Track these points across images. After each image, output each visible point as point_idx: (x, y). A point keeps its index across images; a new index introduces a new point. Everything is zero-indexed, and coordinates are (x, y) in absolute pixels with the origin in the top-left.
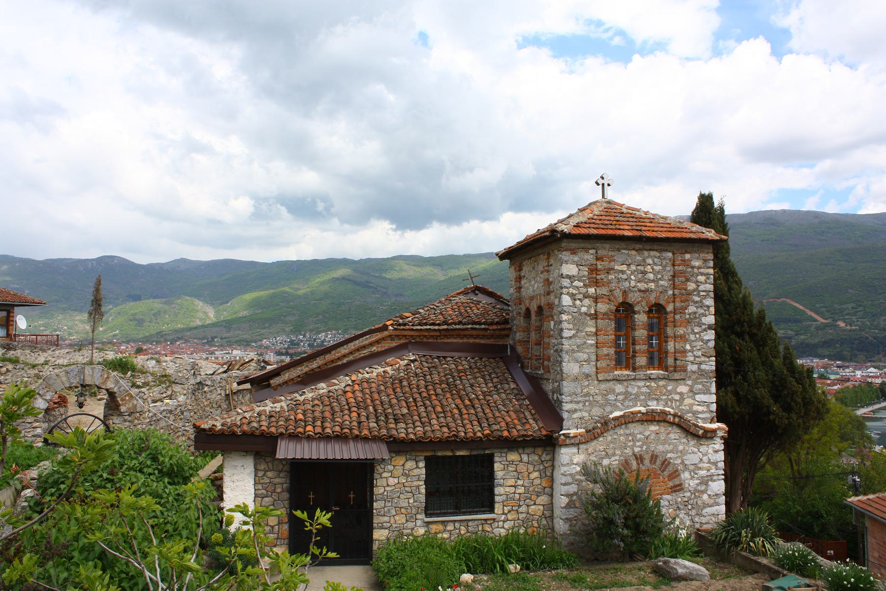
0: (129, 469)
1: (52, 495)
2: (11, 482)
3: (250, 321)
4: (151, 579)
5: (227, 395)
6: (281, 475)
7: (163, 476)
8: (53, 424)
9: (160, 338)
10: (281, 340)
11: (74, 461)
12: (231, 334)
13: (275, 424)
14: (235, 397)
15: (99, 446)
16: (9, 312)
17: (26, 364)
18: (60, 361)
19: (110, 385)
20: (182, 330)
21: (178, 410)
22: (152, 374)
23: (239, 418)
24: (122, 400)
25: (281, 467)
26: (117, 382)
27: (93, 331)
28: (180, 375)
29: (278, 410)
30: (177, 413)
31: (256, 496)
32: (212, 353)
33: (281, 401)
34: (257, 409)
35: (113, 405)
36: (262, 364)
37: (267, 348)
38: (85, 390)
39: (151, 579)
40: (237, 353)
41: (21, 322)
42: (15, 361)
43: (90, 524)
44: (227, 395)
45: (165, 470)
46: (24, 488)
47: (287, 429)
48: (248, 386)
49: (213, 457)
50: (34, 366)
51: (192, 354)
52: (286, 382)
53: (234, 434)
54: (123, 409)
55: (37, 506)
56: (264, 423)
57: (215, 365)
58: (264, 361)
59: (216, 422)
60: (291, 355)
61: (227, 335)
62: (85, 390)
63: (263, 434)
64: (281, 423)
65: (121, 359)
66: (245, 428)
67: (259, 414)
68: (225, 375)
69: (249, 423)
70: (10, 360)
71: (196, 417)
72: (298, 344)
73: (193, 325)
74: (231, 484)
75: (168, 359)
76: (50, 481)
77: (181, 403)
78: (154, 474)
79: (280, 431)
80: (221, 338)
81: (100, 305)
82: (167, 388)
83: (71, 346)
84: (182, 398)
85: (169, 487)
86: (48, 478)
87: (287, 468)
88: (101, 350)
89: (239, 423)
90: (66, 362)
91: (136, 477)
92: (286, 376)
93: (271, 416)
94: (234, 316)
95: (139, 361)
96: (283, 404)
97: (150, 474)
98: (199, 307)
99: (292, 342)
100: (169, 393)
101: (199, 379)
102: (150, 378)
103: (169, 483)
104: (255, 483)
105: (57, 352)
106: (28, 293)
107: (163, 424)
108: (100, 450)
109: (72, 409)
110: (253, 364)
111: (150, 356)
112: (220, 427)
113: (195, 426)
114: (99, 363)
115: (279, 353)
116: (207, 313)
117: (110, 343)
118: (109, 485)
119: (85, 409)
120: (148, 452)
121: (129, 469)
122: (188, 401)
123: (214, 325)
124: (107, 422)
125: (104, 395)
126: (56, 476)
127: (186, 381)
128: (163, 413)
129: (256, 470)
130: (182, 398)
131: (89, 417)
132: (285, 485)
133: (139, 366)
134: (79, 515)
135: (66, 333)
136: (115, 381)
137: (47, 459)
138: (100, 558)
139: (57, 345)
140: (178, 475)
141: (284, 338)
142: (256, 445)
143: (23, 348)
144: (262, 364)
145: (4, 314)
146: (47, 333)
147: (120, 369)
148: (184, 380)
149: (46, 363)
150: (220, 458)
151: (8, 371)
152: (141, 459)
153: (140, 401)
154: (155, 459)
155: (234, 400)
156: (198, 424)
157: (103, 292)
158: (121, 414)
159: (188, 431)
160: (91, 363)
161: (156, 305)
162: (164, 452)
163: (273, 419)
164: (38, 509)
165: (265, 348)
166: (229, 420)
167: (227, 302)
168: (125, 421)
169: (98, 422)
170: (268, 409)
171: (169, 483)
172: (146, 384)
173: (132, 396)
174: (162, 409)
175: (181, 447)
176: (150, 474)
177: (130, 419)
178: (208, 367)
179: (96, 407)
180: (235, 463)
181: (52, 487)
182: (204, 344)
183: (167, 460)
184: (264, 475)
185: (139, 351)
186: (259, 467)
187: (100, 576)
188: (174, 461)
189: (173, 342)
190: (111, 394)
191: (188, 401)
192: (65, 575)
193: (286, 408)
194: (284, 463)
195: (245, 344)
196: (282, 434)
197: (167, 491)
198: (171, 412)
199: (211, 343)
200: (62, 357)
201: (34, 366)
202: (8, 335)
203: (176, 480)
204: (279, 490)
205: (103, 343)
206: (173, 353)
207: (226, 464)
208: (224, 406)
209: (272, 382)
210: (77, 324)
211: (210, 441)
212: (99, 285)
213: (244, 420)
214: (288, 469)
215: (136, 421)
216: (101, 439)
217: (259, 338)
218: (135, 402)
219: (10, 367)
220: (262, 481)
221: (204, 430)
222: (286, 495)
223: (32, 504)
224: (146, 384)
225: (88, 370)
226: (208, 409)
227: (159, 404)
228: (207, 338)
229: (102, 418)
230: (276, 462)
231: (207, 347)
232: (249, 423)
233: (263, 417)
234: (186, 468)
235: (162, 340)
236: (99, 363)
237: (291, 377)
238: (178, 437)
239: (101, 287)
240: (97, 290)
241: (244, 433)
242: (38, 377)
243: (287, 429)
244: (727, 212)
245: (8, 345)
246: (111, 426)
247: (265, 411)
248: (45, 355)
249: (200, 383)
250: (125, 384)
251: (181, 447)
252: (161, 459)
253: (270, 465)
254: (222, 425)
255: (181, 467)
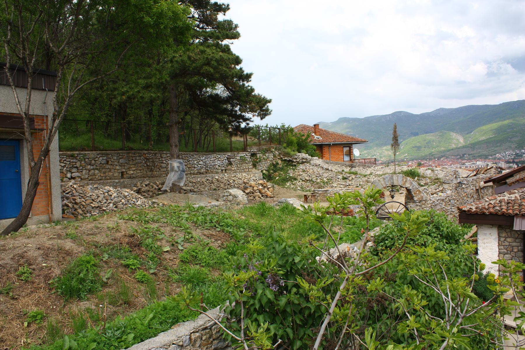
0: (423, 233)
1: (382, 246)
2: (362, 238)
3: (487, 143)
4: (446, 299)
5: (477, 190)
6: (517, 241)
7: (443, 238)
8: (378, 207)
9: (431, 157)
10: (509, 154)
11: (405, 230)
12: (475, 151)
13: (511, 208)
14: (482, 191)
15: (419, 222)
16: (350, 148)
17: (361, 175)
18: (378, 173)
19: (408, 185)
20: (444, 151)
21: (447, 199)
22: (429, 178)
23: (487, 204)
24: (415, 194)
25: (517, 235)
26: (411, 183)
27: (395, 155)
28: (448, 178)
29: (513, 199)
30: (447, 201)
31: (500, 253)
32: (464, 164)
33: (515, 193)
34: (499, 199)
35: (410, 196)
36: (499, 170)
37: (499, 159)
38: (394, 188)
39: (446, 299)
40: (480, 163)
41: (356, 152)
42: (356, 174)
43: (409, 265)
44: (477, 190)
45: (444, 235)
46: (368, 241)
47: (520, 211)
48: (491, 184)
49: (470, 227)
50: (365, 176)
51: (451, 165)
52: (517, 181)
53: (484, 214)
54: (415, 199)
55: (375, 252)
56: (504, 207)
57: (467, 171)
58: (500, 168)
59: (472, 206)
60: (517, 164)
61: (472, 152)
62: (394, 188)
63: (503, 214)
64: (515, 207)
65: (411, 170)
66: (491, 210)
67: (500, 202)
68: (475, 177)
69: (494, 207)
70: (353, 173)
71: (458, 203)
72: (521, 156)
73: (450, 147)
74: (483, 245)
75: (438, 169)
76: (380, 238)
77: (449, 195)
78: (437, 237)
79: (515, 212)
80: (469, 155)
81: (397, 140)
82: (439, 186)
83: (382, 164)
84: (449, 192)
85: (447, 245)
86: (379, 237)
87: (521, 236)
88: (399, 165)
89: (487, 207)
90: (381, 173)
91: (427, 238)
92: (517, 177)
93: (508, 203)
94: (476, 141)
95: (421, 171)
96: (517, 195)
97: (435, 237)
98: (454, 137)
99: (517, 154)
100: (441, 188)
101: (459, 181)
102: (428, 181)
103: (446, 243)
104: (499, 245)
105: (376, 168)
106: (358, 137)
107: (438, 207)
108: (419, 224)
109: (387, 199)
110: (493, 170)
111: (427, 168)
112: (474, 210)
113: (458, 208)
114: (399, 173)
115: (508, 162)
116: (458, 140)
117: (403, 161)
118: (412, 242)
119: (394, 199)
120: (433, 224)
121: (423, 233)
122: (453, 194)
123: (464, 147)
124: (407, 206)
125: (405, 192)
126: (383, 236)
127: (450, 183)
128: (440, 201)
129: (499, 237)
130: (449, 192)
131: (396, 205)
132: (519, 248)
133: (421, 174)
134: (403, 259)
135: (379, 157)
136: (410, 183)
137: (378, 226)
138: (410, 283)
139: (376, 164)
140: (451, 238)
141: (511, 152)
142: (501, 221)
143: (359, 166)
144: (499, 170)
145: (348, 149)
146: (369, 157)
147: (411, 176)
148: (450, 181)
149: (371, 174)
150: (474, 228)
151: (352, 179)
152: (430, 228)
153: (425, 194)
154: (437, 228)
155: (481, 193)
156: (460, 207)
157: (398, 133)
158: (414, 202)
159: (453, 212)
160: (395, 173)
161: (427, 137)
162: (443, 224)
163: (510, 205)
164: (375, 253)
165: (498, 159)
166: (480, 205)
167: (471, 132)
168: (417, 205)
169: (402, 206)
170: (506, 198)
171: (446, 243)
172: (426, 184)
173: (420, 192)
174: (438, 199)
175: (451, 221)
176: (435, 237)
177: (419, 204)
178: (463, 173)
179: (401, 198)
180: (485, 232)
181: (381, 242)
182: (458, 159)
183: (445, 229)
184: (505, 240)
185: (420, 165)
186: (501, 235)
187: (416, 294)
188: (449, 230)
189: (439, 159)
190: (408, 190)
191: (453, 194)
192: (393, 290)
193: (519, 197)
194: (519, 233)
195: (485, 157)
196: (517, 214)
197: (445, 247)
198: (443, 200)
199: (462, 157)
200: (379, 170)
201: (365, 176)
202: (351, 160)
203: (451, 241)
204: (516, 250)
205: (399, 161)
206: (439, 165)
207: (479, 232)
208: (475, 196)
209: (507, 181)
210: (385, 152)
211: (467, 218)
212: (396, 129)
213: (490, 205)
214: (522, 238)
215: (423, 206)
216: (420, 218)
217: (493, 153)
218: (422, 195)
219: (353, 176)
220: (503, 244)
221: (465, 211)
222: (521, 254)
223: (372, 250)
224: (426, 184)
225: (395, 177)
226: (465, 198)
227: (435, 195)
228: (460, 155)
229: (404, 204)
230: (513, 232)
231: (460, 160)
232: (494, 207)
233: (503, 204)
234: (457, 235)
235: (433, 158)
236: (399, 173)
237: (521, 177)
238: (448, 215)
239: (397, 129)
240: (395, 132)
241: (491, 213)
242: (368, 182)
243: (520, 211)
244: (256, 92)
245: (352, 165)
246: (409, 208)
247: (504, 199)
248: (370, 169)
249: (460, 183)
250: (415, 184)
251: (451, 221)
252: (442, 229)
253: (509, 234)
254: (476, 208)
255: (454, 235)
